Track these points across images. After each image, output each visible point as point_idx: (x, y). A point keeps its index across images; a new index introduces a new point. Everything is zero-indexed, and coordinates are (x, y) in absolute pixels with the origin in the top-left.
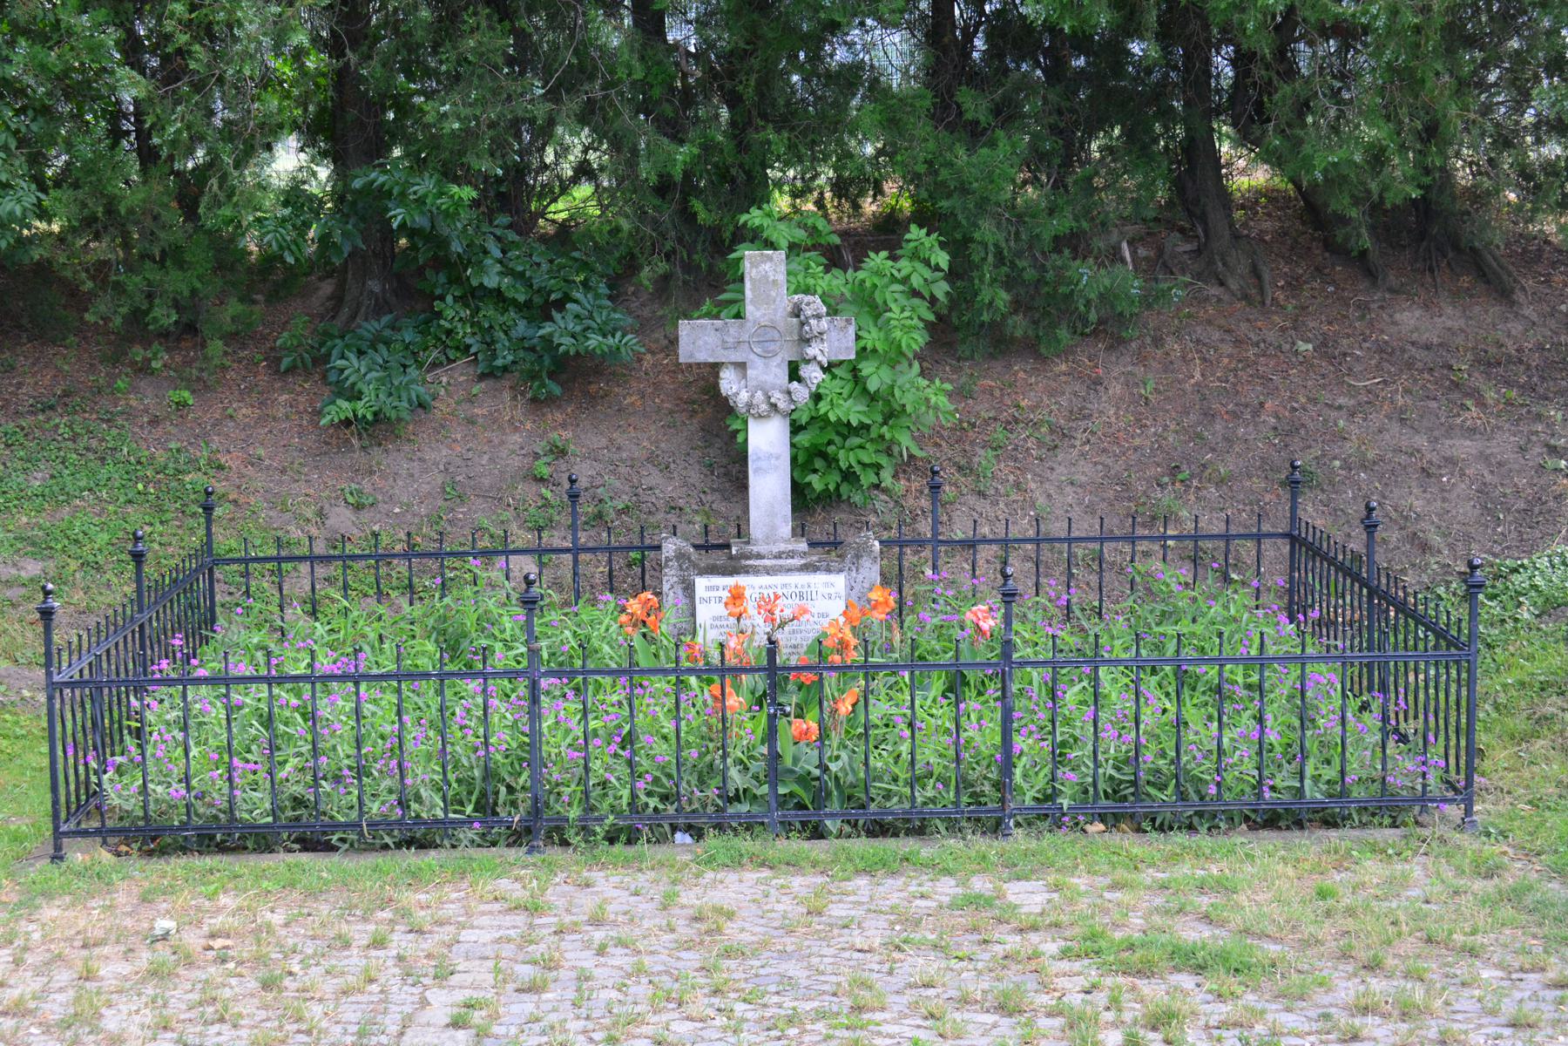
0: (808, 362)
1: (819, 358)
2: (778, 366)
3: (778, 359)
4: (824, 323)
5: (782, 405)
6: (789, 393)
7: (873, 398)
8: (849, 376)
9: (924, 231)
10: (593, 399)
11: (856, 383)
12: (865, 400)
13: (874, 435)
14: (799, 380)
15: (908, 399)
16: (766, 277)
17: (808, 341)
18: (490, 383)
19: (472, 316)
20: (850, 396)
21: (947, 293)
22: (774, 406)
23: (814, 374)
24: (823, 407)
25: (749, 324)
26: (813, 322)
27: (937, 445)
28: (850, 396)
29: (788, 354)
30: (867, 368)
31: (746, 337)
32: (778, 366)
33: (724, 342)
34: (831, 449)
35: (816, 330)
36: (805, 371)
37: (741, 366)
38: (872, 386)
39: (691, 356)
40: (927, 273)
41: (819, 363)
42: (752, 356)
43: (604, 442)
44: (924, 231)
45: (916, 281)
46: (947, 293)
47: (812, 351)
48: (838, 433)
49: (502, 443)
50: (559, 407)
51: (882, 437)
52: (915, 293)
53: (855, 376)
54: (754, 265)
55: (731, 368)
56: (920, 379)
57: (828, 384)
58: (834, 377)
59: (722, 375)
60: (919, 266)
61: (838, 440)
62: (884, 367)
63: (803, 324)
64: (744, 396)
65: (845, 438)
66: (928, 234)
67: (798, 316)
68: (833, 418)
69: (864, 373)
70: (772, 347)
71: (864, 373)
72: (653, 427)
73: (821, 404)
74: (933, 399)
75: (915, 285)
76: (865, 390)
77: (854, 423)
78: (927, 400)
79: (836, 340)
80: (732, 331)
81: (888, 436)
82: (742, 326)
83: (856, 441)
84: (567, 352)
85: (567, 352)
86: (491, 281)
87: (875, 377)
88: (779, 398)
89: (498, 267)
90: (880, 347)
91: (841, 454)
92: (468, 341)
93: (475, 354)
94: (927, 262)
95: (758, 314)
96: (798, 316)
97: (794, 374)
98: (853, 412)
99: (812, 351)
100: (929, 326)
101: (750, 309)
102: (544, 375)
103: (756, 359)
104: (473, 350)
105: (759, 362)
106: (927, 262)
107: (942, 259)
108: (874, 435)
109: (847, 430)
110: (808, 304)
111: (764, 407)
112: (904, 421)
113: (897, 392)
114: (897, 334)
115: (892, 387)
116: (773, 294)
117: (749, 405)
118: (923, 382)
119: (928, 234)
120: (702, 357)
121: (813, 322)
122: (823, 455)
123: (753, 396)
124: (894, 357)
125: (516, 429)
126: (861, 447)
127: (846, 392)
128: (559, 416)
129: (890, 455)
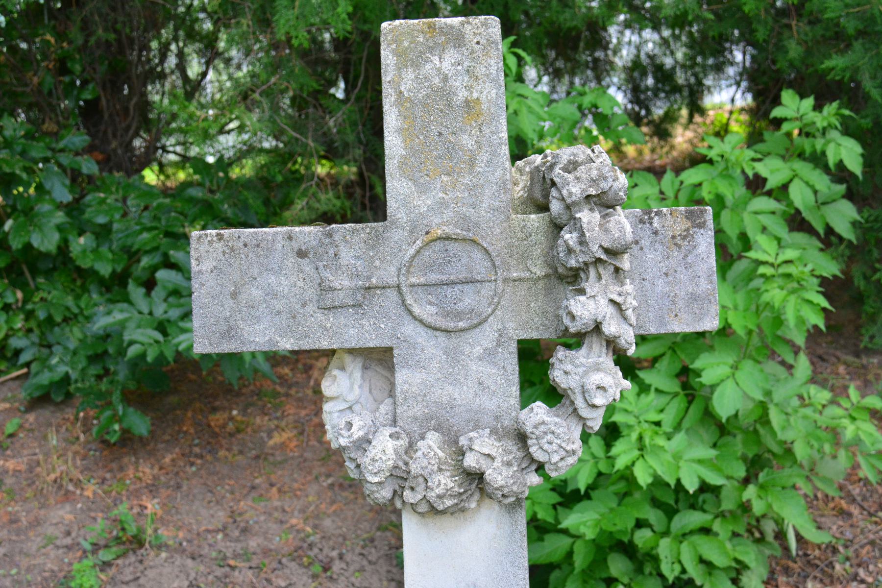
0: (574, 340)
1: (611, 328)
2: (489, 355)
3: (486, 337)
4: (622, 223)
5: (498, 476)
6: (522, 438)
7: (722, 430)
8: (674, 386)
9: (809, 102)
10: (212, 439)
11: (691, 399)
12: (708, 434)
13: (728, 504)
14: (554, 396)
15: (790, 429)
16: (444, 93)
17: (572, 279)
18: (46, 413)
19: (25, 301)
20: (678, 427)
21: (854, 224)
22: (476, 479)
23: (589, 376)
24: (623, 453)
25: (397, 235)
26: (588, 217)
27: (844, 514)
28: (678, 427)
29: (519, 320)
30: (712, 368)
31: (388, 274)
32: (489, 355)
33: (324, 288)
34: (642, 538)
35: (597, 239)
36: (566, 369)
37: (380, 359)
38: (726, 404)
39: (230, 332)
40: (822, 182)
41: (612, 344)
42: (410, 329)
43: (222, 516)
44: (809, 102)
45: (799, 196)
46: (854, 224)
47: (588, 306)
48: (656, 503)
49: (36, 523)
50: (152, 453)
51: (746, 507)
52: (797, 222)
53: (685, 386)
54: (412, 59)
55: (355, 367)
56: (813, 389)
57: (632, 403)
58: (643, 388)
59: (328, 387)
60: (804, 169)
61: (653, 516)
62: (748, 366)
63: (557, 227)
64: (384, 450)
65: (670, 512)
66: (818, 107)
67: (544, 208)
68: (643, 478)
69: (707, 378)
70: (468, 299)
71: (707, 378)
72: (313, 489)
73: (618, 447)
74: (849, 431)
75: (798, 203)
76: (708, 414)
77: (691, 486)
78: (835, 433)
79: (662, 278)
80: (347, 255)
81: (758, 508)
82: (377, 240)
83: (692, 519)
84: (143, 356)
85: (143, 356)
86: (45, 241)
87: (729, 385)
88: (487, 452)
89: (60, 217)
90: (738, 325)
91: (664, 549)
92: (16, 342)
93: (28, 365)
94: (818, 160)
95: (424, 203)
96: (544, 208)
97: (534, 367)
98: (687, 461)
99: (588, 306)
100: (828, 286)
101: (397, 187)
102: (116, 397)
103: (421, 336)
104: (24, 358)
105: (431, 346)
106: (818, 160)
107: (848, 153)
108: (728, 504)
109: (670, 499)
110: (572, 166)
111: (444, 482)
112: (789, 475)
113: (775, 417)
114: (774, 294)
115: (763, 407)
116: (467, 141)
117: (401, 477)
118: (822, 396)
119: (818, 107)
120: (260, 336)
121: (588, 217)
122: (627, 549)
123: (411, 447)
124: (765, 344)
125: (67, 497)
126: (706, 531)
127: (668, 419)
128: (147, 471)
129: (761, 540)
